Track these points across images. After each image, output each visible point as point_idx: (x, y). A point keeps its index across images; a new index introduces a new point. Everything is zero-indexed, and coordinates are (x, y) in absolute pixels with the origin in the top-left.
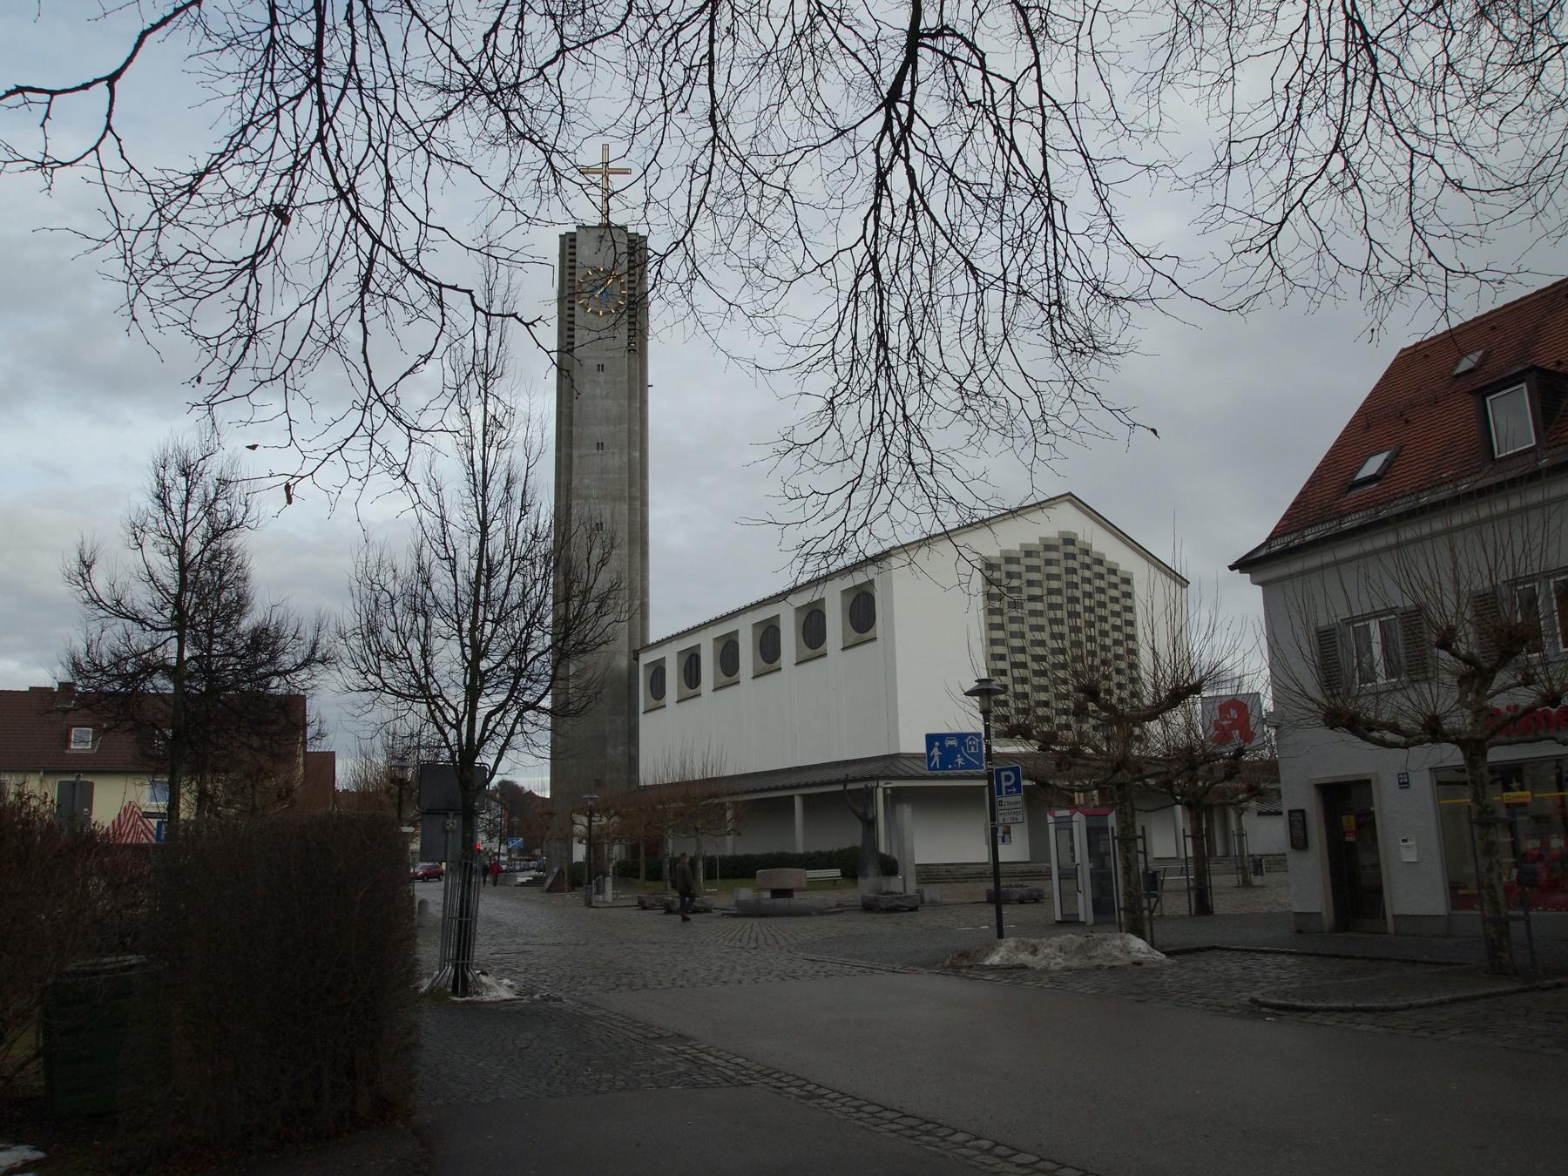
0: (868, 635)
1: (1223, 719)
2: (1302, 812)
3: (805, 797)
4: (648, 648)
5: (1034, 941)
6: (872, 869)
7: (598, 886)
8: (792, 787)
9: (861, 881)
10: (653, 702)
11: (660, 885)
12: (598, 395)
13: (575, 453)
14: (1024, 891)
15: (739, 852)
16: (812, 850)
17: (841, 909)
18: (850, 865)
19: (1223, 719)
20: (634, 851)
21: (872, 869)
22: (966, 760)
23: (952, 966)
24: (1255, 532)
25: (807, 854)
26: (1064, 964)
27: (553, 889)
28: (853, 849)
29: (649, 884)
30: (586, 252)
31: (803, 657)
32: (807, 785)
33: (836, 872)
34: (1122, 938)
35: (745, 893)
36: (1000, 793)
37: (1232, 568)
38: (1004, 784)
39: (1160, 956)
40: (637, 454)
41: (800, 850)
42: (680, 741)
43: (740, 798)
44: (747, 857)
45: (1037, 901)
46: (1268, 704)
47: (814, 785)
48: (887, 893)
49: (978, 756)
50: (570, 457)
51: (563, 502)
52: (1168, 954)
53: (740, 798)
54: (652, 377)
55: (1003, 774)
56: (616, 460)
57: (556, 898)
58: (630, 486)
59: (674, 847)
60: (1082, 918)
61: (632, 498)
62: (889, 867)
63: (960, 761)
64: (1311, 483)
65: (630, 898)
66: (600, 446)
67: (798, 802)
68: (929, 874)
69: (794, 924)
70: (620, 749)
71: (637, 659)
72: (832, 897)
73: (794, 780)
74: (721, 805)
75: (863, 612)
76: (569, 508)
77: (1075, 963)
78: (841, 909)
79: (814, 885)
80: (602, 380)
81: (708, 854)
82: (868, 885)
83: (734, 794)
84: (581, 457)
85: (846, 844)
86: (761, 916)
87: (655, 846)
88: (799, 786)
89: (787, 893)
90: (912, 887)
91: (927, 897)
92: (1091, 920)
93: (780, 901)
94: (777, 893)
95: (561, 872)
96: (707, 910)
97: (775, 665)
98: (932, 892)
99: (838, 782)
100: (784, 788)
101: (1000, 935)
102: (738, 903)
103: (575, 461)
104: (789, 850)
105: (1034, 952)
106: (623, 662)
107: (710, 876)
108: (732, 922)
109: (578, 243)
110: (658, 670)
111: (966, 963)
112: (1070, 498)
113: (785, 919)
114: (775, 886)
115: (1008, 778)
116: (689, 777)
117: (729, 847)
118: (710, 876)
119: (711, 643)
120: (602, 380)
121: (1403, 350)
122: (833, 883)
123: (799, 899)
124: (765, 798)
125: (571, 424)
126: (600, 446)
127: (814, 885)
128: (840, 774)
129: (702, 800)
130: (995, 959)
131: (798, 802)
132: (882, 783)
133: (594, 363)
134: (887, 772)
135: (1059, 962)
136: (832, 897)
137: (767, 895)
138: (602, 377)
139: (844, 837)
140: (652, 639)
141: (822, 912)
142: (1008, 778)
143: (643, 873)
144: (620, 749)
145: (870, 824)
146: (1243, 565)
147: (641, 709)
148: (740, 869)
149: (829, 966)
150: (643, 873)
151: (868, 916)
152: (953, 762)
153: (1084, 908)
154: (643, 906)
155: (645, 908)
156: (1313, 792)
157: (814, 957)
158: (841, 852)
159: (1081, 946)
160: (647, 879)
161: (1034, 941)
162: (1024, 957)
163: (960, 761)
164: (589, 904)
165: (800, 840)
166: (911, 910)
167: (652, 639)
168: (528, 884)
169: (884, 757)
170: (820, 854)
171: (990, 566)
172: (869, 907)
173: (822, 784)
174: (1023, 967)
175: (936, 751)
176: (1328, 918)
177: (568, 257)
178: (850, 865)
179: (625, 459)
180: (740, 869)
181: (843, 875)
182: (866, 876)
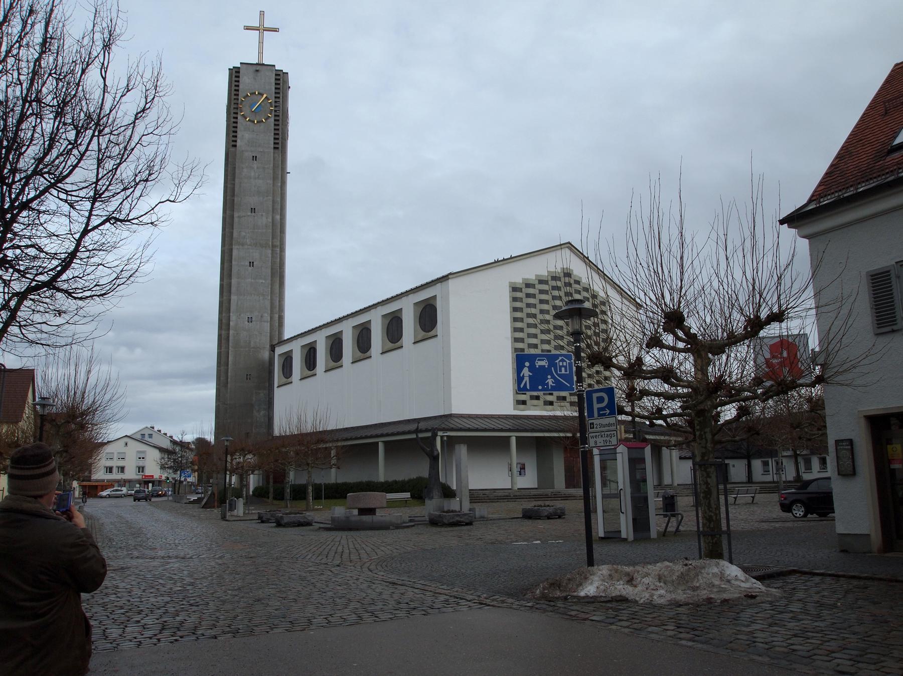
0: (432, 333)
1: (773, 357)
2: (851, 442)
3: (386, 443)
4: (282, 342)
5: (627, 569)
6: (436, 493)
7: (230, 505)
8: (377, 436)
9: (427, 502)
10: (284, 380)
11: (282, 503)
12: (253, 177)
13: (236, 215)
14: (551, 510)
15: (340, 481)
16: (390, 480)
17: (413, 523)
18: (419, 490)
19: (773, 357)
20: (266, 478)
21: (436, 493)
22: (556, 381)
23: (544, 597)
24: (799, 196)
25: (386, 482)
26: (669, 597)
27: (205, 507)
28: (420, 479)
29: (275, 502)
30: (246, 80)
31: (386, 349)
32: (388, 435)
33: (407, 495)
34: (717, 565)
35: (339, 511)
36: (591, 415)
37: (782, 222)
38: (596, 406)
39: (758, 585)
40: (278, 217)
41: (382, 479)
42: (301, 405)
43: (339, 444)
44: (345, 484)
45: (560, 517)
46: (814, 343)
47: (393, 434)
48: (448, 511)
49: (568, 377)
50: (232, 217)
51: (227, 247)
52: (759, 578)
53: (339, 444)
54: (289, 168)
55: (595, 396)
56: (264, 220)
57: (205, 513)
58: (273, 238)
59: (293, 477)
60: (624, 535)
61: (273, 246)
62: (448, 493)
63: (550, 381)
64: (840, 157)
65: (255, 511)
66: (253, 210)
67: (381, 447)
68: (477, 496)
69: (375, 537)
70: (262, 413)
71: (274, 351)
72: (402, 514)
73: (379, 432)
74: (328, 450)
75: (428, 316)
76: (231, 250)
77: (681, 595)
78: (413, 523)
79: (392, 504)
80: (255, 166)
81: (316, 482)
82: (432, 506)
83: (337, 441)
84: (239, 217)
85: (414, 475)
86: (350, 529)
87: (279, 477)
88: (382, 435)
89: (371, 511)
90: (466, 506)
91: (478, 514)
92: (631, 537)
93: (366, 518)
94: (363, 511)
95: (213, 494)
96: (308, 524)
97: (368, 354)
98: (481, 510)
99: (409, 432)
100: (371, 437)
101: (591, 562)
102: (333, 520)
103: (236, 220)
104: (374, 479)
105: (631, 581)
106: (266, 355)
107: (317, 497)
108: (325, 534)
109: (241, 75)
110: (287, 359)
111: (558, 593)
112: (570, 246)
113: (369, 533)
114: (362, 506)
115: (600, 400)
116: (305, 432)
117: (333, 477)
118: (317, 497)
119: (324, 339)
120: (255, 166)
121: (897, 65)
122: (404, 503)
123: (381, 515)
124: (358, 444)
125: (233, 195)
126: (253, 210)
127: (392, 504)
128: (413, 427)
129: (315, 445)
130: (590, 589)
131: (381, 447)
132: (440, 433)
133: (251, 155)
134: (443, 426)
135: (662, 595)
136: (402, 514)
137: (356, 512)
138: (255, 165)
139: (419, 469)
140: (287, 336)
141: (398, 527)
142: (600, 400)
143: (271, 495)
144: (262, 413)
145: (434, 459)
146: (791, 220)
147: (276, 385)
148: (337, 492)
149: (410, 593)
150: (271, 495)
151: (435, 530)
152: (543, 383)
153: (626, 528)
154: (262, 520)
155: (263, 522)
156: (863, 423)
157: (393, 578)
158: (410, 481)
159: (682, 576)
160: (275, 498)
161: (627, 569)
162: (621, 588)
163: (550, 381)
164: (224, 518)
165: (382, 472)
166: (467, 524)
167: (287, 336)
168: (194, 502)
169: (441, 417)
170: (396, 482)
171: (514, 289)
172: (434, 522)
173: (398, 434)
174: (622, 600)
175: (526, 372)
176: (876, 538)
177: (234, 79)
178: (419, 490)
179: (270, 220)
180: (337, 492)
181: (412, 496)
182: (431, 498)
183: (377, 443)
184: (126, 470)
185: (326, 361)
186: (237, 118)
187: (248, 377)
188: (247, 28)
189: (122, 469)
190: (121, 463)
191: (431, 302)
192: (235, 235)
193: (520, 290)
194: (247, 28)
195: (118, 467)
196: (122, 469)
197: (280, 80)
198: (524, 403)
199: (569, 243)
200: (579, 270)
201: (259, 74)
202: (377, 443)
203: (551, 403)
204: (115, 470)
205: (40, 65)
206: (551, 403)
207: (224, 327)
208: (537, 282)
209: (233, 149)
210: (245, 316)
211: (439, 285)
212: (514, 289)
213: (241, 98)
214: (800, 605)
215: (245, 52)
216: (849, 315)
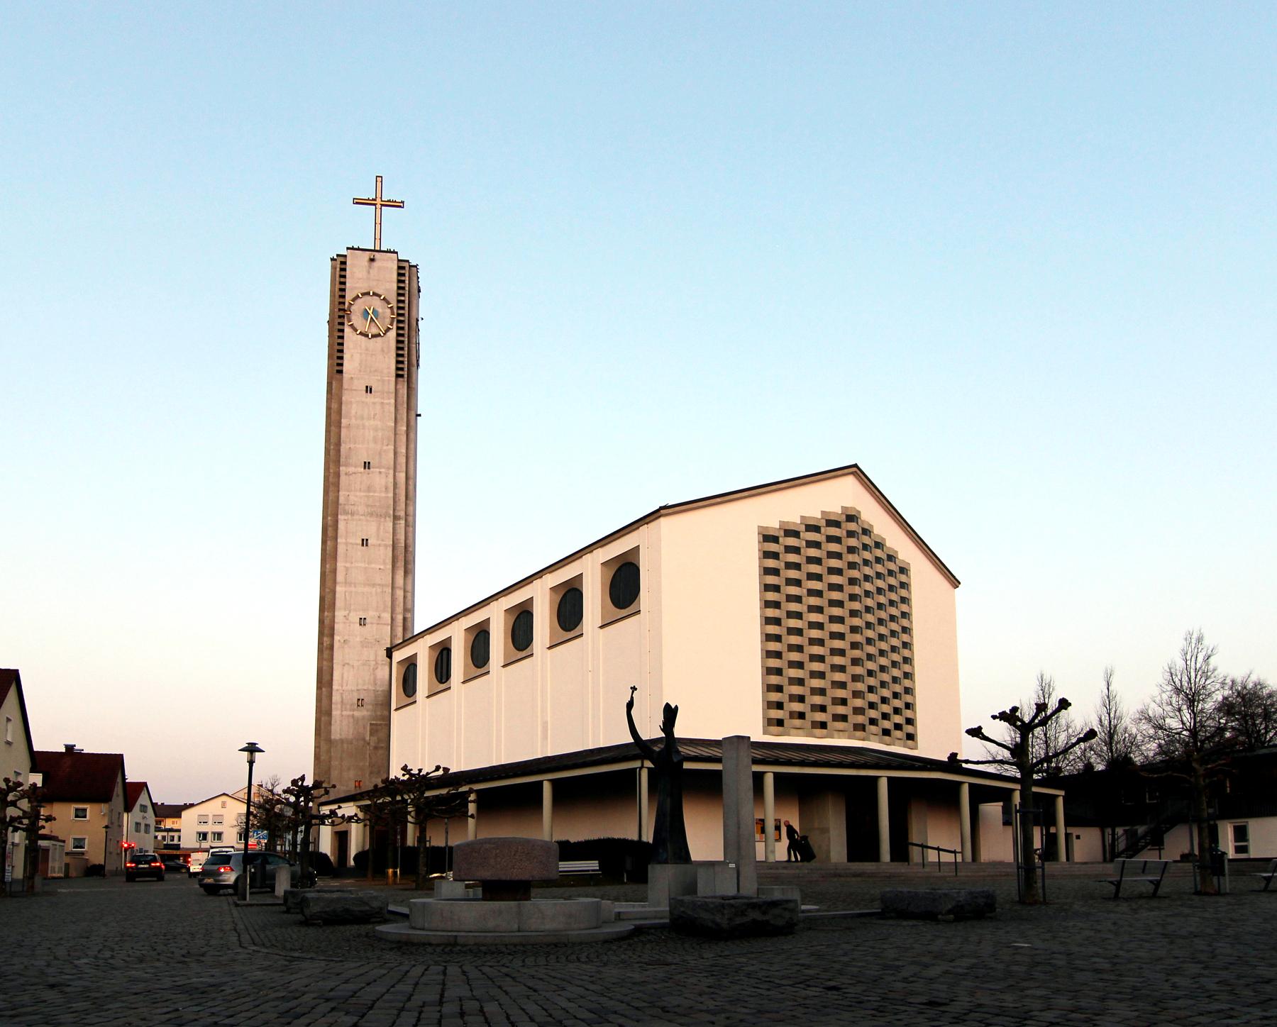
4: (407, 641)
30: (357, 280)
50: (338, 475)
75: (625, 584)
112: (854, 470)
124: (507, 790)
126: (367, 465)
147: (394, 706)
171: (768, 538)
183: (541, 783)
184: (224, 836)
185: (466, 665)
186: (342, 331)
187: (360, 703)
188: (358, 202)
189: (219, 836)
190: (218, 829)
191: (631, 559)
192: (342, 500)
193: (775, 539)
194: (358, 202)
195: (214, 833)
196: (219, 836)
197: (406, 273)
198: (780, 723)
199: (856, 466)
200: (872, 515)
201: (375, 264)
202: (541, 783)
203: (823, 725)
204: (209, 836)
205: (329, 741)
206: (823, 725)
207: (326, 632)
208: (803, 528)
209: (338, 376)
210: (355, 618)
211: (644, 529)
212: (768, 538)
213: (348, 299)
214: (477, 1004)
215: (357, 229)
216: (994, 761)
